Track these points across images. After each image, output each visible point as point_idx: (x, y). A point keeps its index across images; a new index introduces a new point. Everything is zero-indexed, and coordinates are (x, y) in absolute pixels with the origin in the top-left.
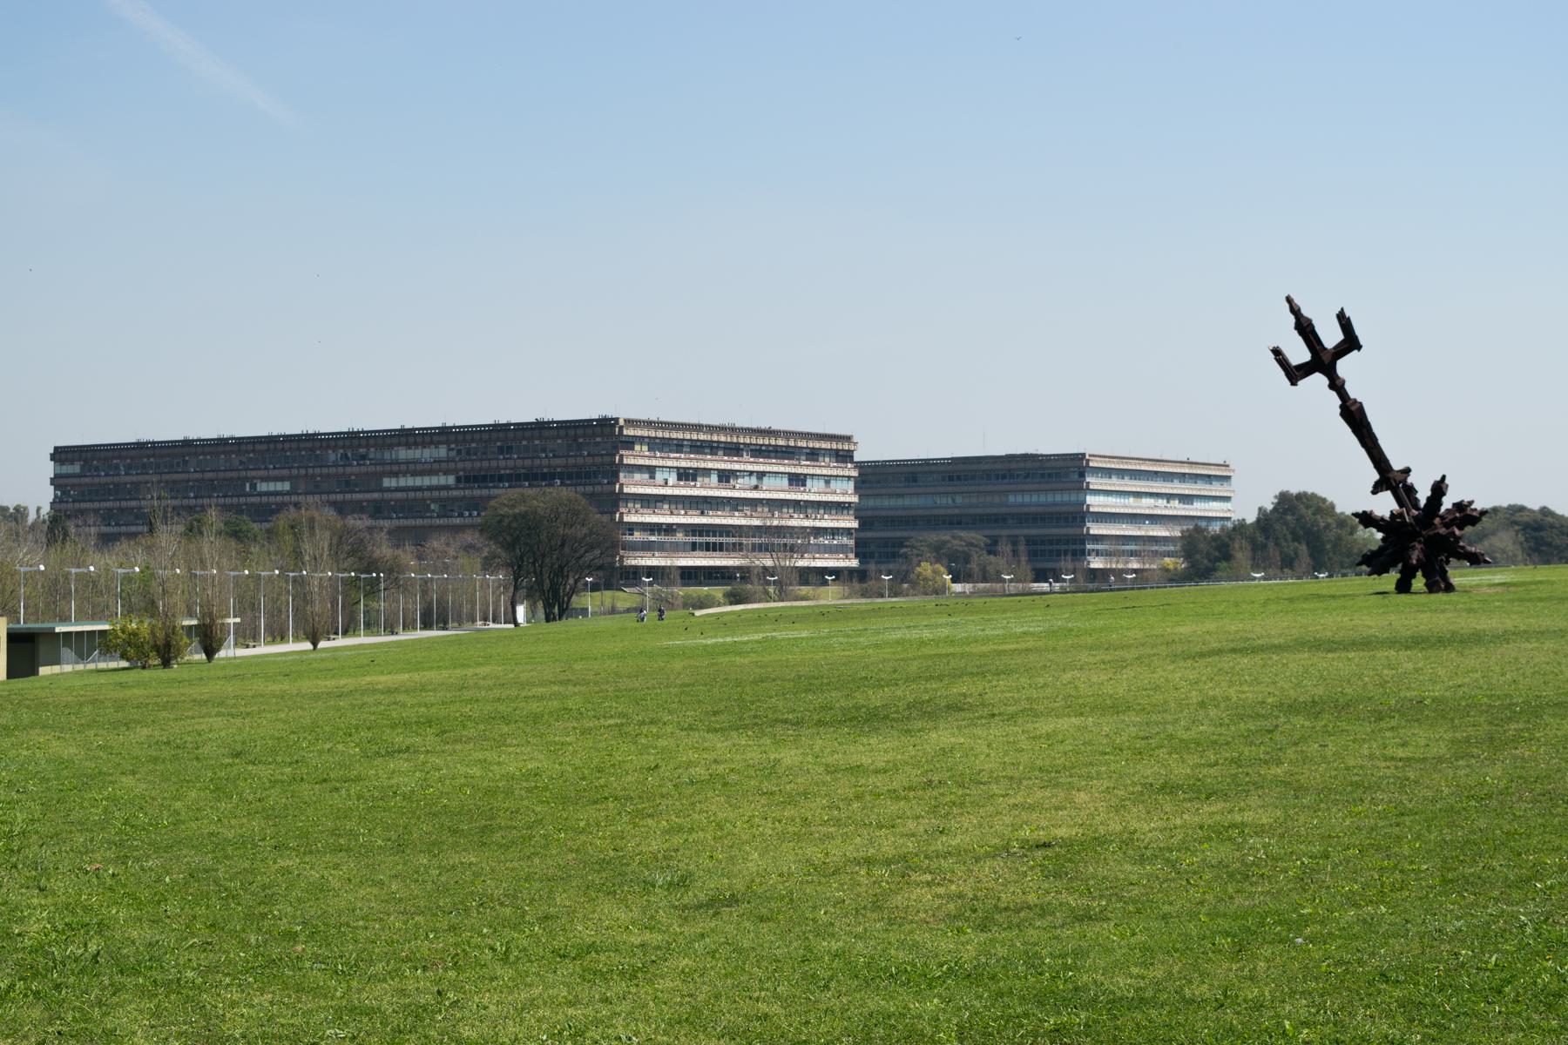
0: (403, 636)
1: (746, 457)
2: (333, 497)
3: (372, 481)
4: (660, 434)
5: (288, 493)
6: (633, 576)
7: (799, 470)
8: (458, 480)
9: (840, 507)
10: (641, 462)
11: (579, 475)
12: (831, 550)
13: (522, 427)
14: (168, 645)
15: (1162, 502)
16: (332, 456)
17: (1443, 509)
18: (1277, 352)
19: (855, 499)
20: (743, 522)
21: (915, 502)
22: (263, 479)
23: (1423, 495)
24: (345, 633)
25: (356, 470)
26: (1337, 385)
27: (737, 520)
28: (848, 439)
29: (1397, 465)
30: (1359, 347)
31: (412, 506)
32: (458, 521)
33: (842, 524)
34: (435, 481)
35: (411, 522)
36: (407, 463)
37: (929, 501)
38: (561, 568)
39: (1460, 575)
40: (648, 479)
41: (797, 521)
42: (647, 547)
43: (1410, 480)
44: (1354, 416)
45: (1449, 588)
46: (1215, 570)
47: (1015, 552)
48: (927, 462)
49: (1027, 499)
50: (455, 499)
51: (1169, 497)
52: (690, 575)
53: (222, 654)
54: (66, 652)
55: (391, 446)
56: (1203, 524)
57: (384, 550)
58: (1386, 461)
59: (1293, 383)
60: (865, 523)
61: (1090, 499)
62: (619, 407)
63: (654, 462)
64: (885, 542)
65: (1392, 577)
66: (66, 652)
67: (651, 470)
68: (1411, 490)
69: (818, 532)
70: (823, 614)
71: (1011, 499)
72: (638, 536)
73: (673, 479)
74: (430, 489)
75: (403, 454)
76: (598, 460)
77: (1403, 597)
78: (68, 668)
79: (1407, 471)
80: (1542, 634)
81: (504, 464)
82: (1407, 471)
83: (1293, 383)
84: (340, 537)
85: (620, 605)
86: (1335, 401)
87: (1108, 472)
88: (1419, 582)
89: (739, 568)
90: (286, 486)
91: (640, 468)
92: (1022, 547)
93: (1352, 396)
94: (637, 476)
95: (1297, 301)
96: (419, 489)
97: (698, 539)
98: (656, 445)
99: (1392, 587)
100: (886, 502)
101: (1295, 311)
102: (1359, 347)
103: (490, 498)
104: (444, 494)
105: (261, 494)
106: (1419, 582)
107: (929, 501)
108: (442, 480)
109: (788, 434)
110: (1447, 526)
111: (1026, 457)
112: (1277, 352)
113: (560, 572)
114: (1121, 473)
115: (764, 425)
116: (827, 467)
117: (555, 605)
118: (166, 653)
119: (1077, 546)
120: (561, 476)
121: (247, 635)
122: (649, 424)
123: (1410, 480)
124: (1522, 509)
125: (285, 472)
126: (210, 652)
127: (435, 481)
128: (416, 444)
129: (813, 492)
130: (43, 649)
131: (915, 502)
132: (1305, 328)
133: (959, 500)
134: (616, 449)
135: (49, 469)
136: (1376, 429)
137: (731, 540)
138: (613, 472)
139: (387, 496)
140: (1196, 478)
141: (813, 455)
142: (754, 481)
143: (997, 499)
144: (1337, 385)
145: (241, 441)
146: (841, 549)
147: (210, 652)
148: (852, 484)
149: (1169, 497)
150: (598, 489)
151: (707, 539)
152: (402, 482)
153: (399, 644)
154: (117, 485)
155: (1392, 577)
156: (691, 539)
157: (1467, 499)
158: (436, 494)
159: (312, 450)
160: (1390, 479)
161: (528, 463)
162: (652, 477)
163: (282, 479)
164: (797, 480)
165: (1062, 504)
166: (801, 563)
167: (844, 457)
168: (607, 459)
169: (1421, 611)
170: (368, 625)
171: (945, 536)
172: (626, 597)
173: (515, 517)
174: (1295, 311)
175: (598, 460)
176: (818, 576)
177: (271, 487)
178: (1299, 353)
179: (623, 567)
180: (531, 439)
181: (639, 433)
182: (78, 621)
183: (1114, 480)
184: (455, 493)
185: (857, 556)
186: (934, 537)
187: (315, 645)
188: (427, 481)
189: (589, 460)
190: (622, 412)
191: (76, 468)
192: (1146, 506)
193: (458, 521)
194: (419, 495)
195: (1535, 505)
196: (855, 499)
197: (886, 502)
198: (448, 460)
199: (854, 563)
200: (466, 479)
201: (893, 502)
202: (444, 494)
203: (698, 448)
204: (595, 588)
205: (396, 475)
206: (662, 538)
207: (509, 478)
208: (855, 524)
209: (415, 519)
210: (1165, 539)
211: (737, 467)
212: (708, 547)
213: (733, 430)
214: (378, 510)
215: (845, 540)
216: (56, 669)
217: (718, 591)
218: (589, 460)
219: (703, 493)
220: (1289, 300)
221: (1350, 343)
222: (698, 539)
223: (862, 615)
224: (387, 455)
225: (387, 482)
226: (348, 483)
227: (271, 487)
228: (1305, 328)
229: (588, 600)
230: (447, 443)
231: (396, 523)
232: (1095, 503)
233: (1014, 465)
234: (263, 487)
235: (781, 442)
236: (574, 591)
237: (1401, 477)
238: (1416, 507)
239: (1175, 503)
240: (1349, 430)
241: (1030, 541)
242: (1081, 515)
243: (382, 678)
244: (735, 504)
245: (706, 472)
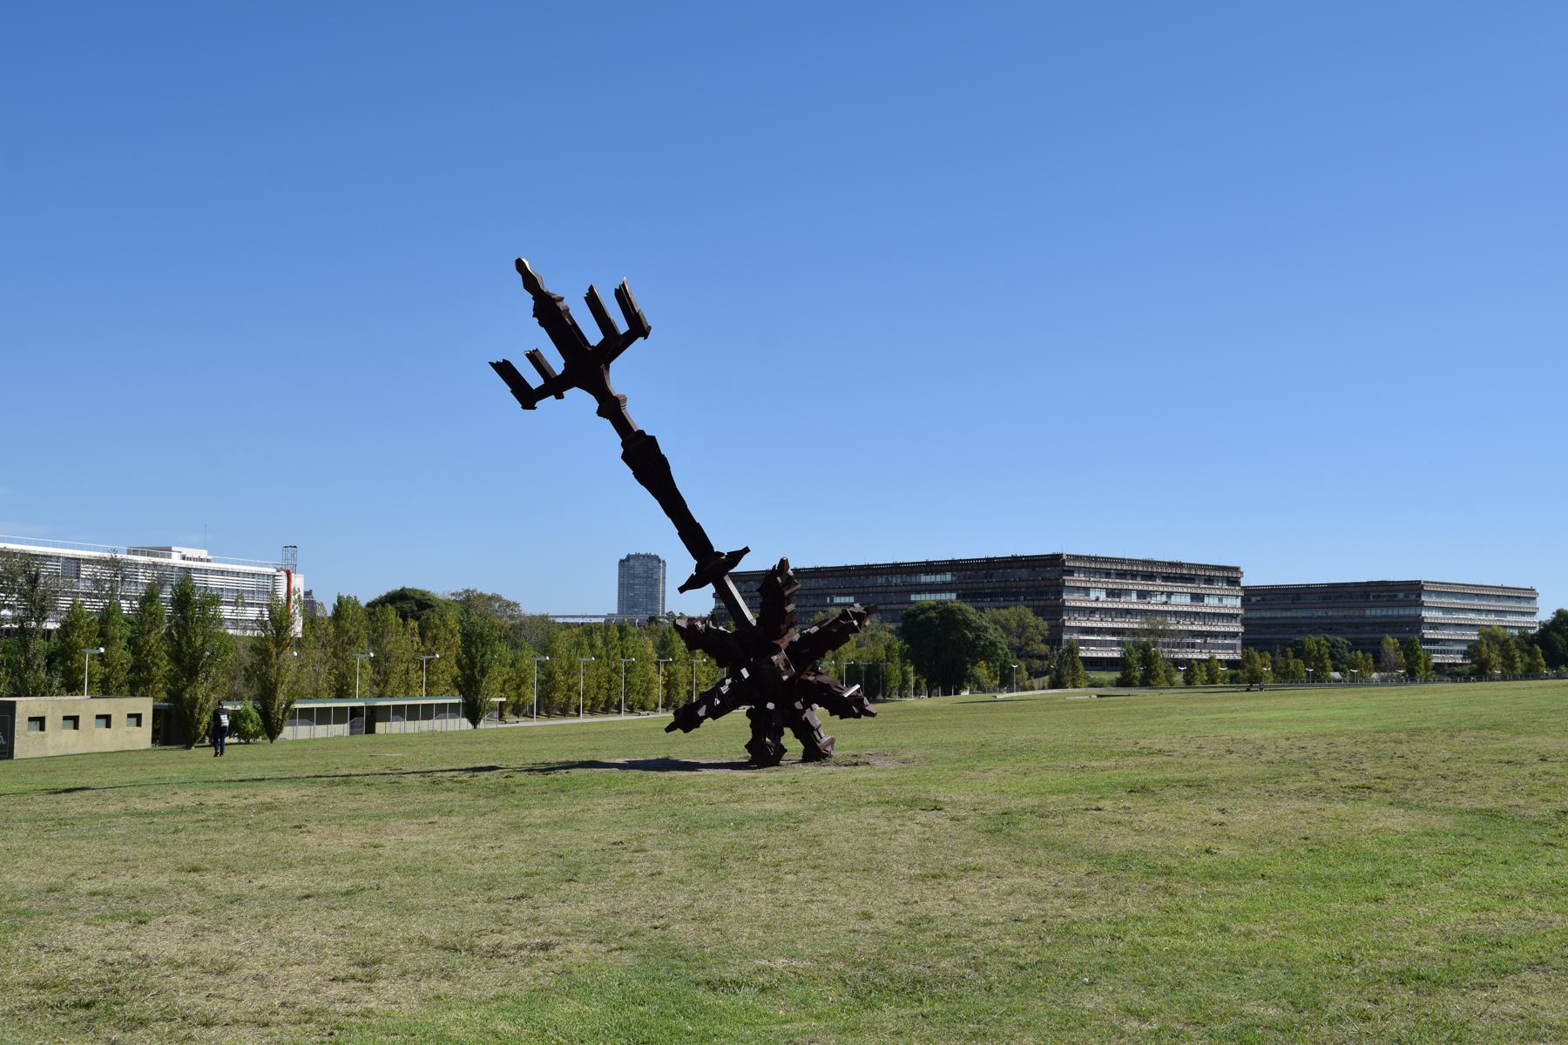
1: (1159, 582)
9: (1232, 617)
26: (611, 408)
28: (1236, 569)
40: (1087, 596)
44: (646, 461)
55: (867, 576)
71: (1368, 612)
73: (1103, 596)
75: (924, 579)
91: (1078, 588)
94: (1076, 596)
101: (530, 282)
109: (1191, 566)
132: (549, 311)
138: (1059, 589)
142: (1164, 598)
144: (611, 408)
146: (1233, 647)
160: (712, 566)
164: (1142, 595)
167: (1234, 582)
174: (530, 282)
182: (330, 699)
201: (1285, 614)
203: (1122, 575)
205: (918, 592)
220: (520, 265)
224: (866, 583)
225: (913, 597)
228: (549, 311)
242: (1419, 623)
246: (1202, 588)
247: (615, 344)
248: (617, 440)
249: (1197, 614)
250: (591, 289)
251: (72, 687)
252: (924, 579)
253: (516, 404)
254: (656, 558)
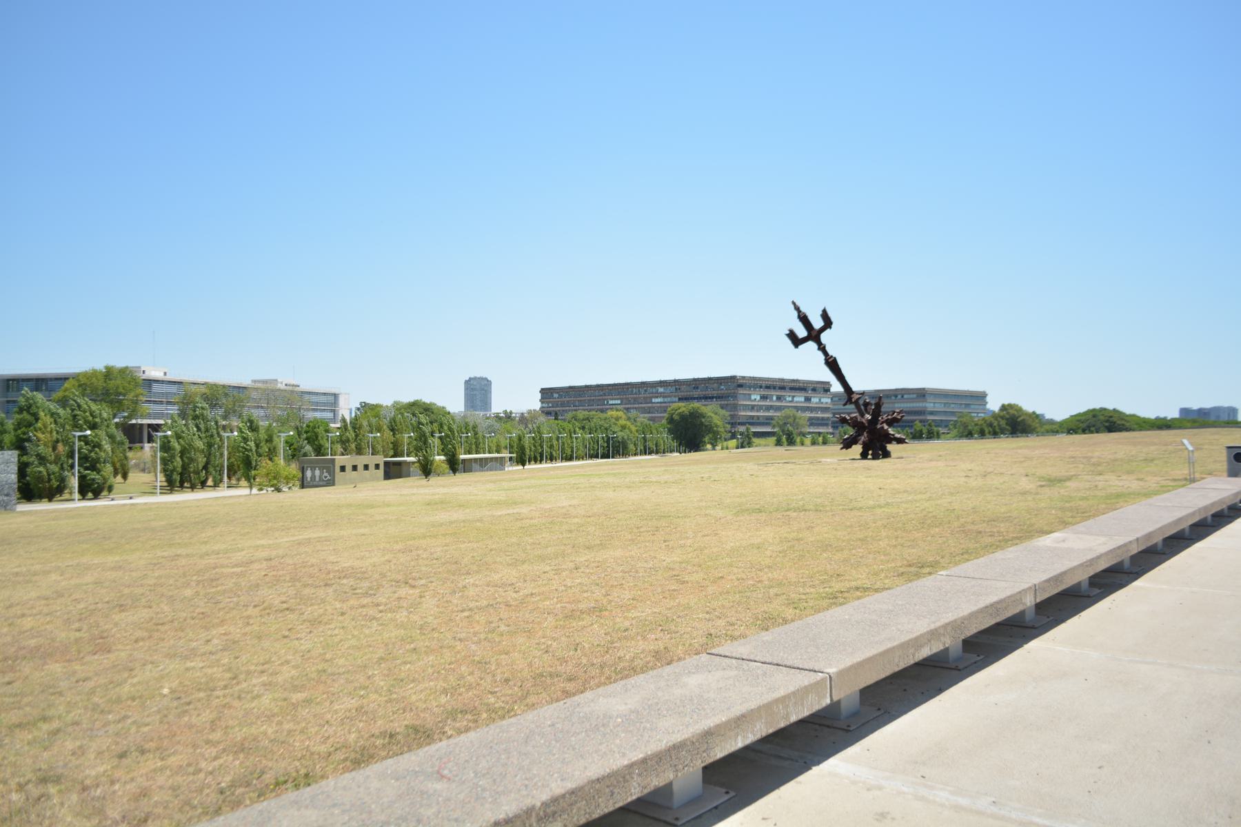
3: (648, 400)
9: (825, 410)
26: (822, 348)
81: (696, 393)
101: (797, 309)
132: (804, 319)
135: (539, 396)
144: (822, 348)
153: (117, 506)
174: (797, 309)
178: (802, 332)
195: (1111, 408)
203: (768, 387)
220: (794, 303)
221: (828, 323)
228: (804, 319)
246: (810, 394)
247: (823, 330)
250: (824, 312)
251: (359, 451)
253: (792, 346)
254: (466, 382)
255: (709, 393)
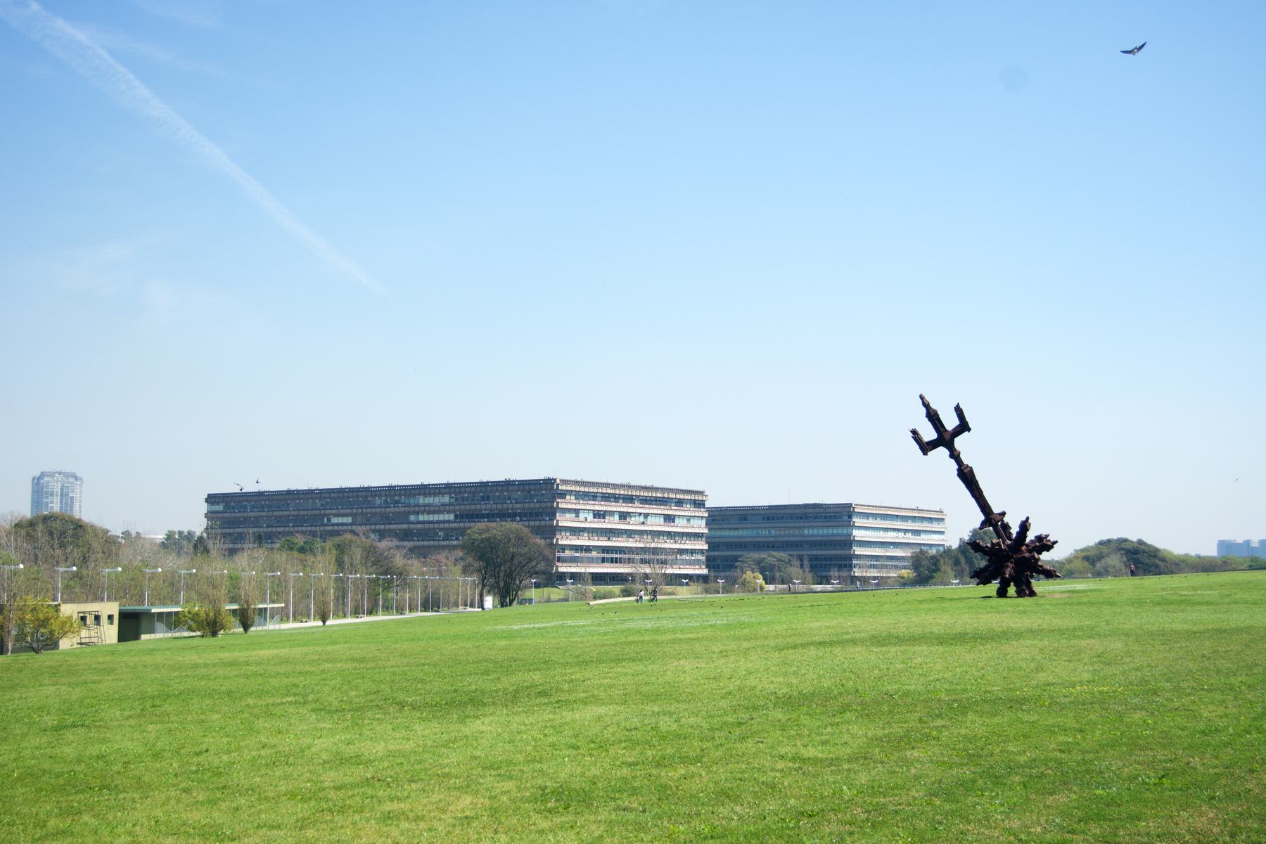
0: (408, 615)
1: (637, 504)
2: (378, 527)
3: (403, 517)
4: (582, 489)
5: (351, 524)
6: (562, 578)
7: (671, 513)
8: (456, 517)
9: (697, 536)
10: (570, 506)
11: (531, 515)
12: (690, 563)
13: (497, 484)
14: (215, 622)
15: (901, 534)
16: (378, 501)
17: (1028, 540)
18: (914, 432)
19: (706, 531)
20: (634, 545)
21: (745, 533)
22: (335, 515)
23: (1015, 530)
24: (370, 613)
25: (392, 510)
26: (955, 455)
27: (630, 543)
28: (702, 493)
29: (996, 509)
30: (969, 430)
31: (427, 533)
32: (455, 543)
33: (698, 547)
34: (441, 517)
35: (426, 543)
36: (425, 506)
37: (754, 533)
38: (511, 572)
39: (1039, 585)
40: (574, 517)
41: (670, 545)
42: (573, 560)
43: (1006, 519)
44: (967, 477)
45: (1032, 594)
46: (932, 577)
47: (802, 566)
48: (753, 508)
49: (816, 532)
50: (454, 529)
51: (906, 531)
52: (598, 578)
53: (253, 629)
54: (158, 625)
55: (414, 496)
56: (924, 548)
57: (399, 561)
58: (989, 507)
59: (925, 454)
60: (713, 546)
61: (855, 532)
62: (557, 472)
63: (578, 507)
64: (726, 558)
65: (995, 585)
66: (158, 625)
67: (577, 512)
68: (1006, 527)
69: (681, 551)
70: (683, 603)
71: (806, 532)
72: (568, 553)
73: (590, 517)
74: (438, 522)
76: (543, 505)
77: (1003, 600)
78: (159, 636)
79: (1003, 514)
80: (1033, 633)
81: (485, 507)
82: (1003, 514)
83: (925, 454)
84: (370, 551)
85: (553, 597)
86: (954, 466)
87: (867, 515)
88: (1012, 590)
89: (631, 574)
90: (349, 520)
91: (569, 510)
92: (806, 562)
93: (965, 462)
94: (568, 516)
95: (927, 398)
96: (432, 522)
97: (605, 555)
98: (580, 496)
99: (994, 593)
100: (727, 533)
102: (969, 430)
103: (465, 529)
104: (447, 525)
105: (334, 525)
106: (1012, 590)
107: (754, 533)
108: (447, 517)
109: (664, 490)
110: (1030, 551)
111: (815, 506)
112: (914, 432)
113: (510, 576)
114: (875, 516)
115: (649, 484)
116: (688, 510)
117: (507, 596)
118: (212, 627)
119: (846, 562)
120: (520, 515)
121: (336, 615)
122: (577, 483)
123: (1006, 519)
124: (1126, 540)
125: (349, 511)
126: (246, 627)
127: (441, 517)
128: (430, 494)
129: (680, 526)
130: (144, 623)
131: (745, 533)
132: (933, 417)
133: (773, 532)
134: (554, 498)
135: (204, 508)
136: (982, 485)
137: (627, 556)
139: (412, 526)
140: (922, 519)
141: (680, 503)
142: (642, 519)
143: (797, 532)
144: (955, 455)
145: (322, 491)
146: (697, 562)
147: (246, 627)
148: (704, 522)
149: (906, 531)
150: (543, 523)
151: (612, 555)
152: (421, 518)
154: (245, 518)
155: (995, 585)
156: (602, 555)
157: (1044, 534)
158: (442, 526)
159: (366, 497)
161: (500, 506)
162: (577, 516)
163: (346, 515)
164: (669, 519)
165: (838, 535)
166: (669, 571)
167: (699, 504)
168: (549, 505)
169: (1011, 612)
170: (294, 617)
171: (763, 555)
172: (556, 592)
173: (482, 541)
175: (543, 505)
176: (676, 580)
177: (340, 520)
178: (929, 434)
179: (557, 572)
180: (502, 491)
181: (569, 488)
183: (871, 520)
184: (454, 525)
185: (707, 567)
186: (756, 555)
187: (324, 622)
188: (436, 517)
189: (538, 505)
190: (558, 476)
191: (220, 508)
192: (891, 537)
193: (455, 543)
194: (431, 526)
195: (1134, 538)
196: (706, 531)
197: (727, 533)
198: (450, 504)
199: (705, 571)
200: (460, 517)
201: (731, 533)
202: (447, 525)
203: (606, 498)
204: (537, 586)
206: (584, 555)
207: (488, 516)
208: (706, 547)
209: (423, 541)
210: (902, 557)
211: (631, 510)
212: (613, 561)
213: (629, 487)
214: (405, 535)
215: (699, 557)
216: (152, 636)
217: (616, 589)
218: (538, 505)
219: (609, 526)
220: (922, 397)
221: (963, 427)
222: (605, 555)
223: (702, 604)
224: (412, 501)
226: (388, 518)
227: (340, 520)
228: (933, 417)
229: (533, 593)
230: (449, 493)
231: (412, 544)
232: (858, 535)
233: (808, 511)
234: (335, 520)
235: (659, 495)
236: (519, 588)
237: (999, 518)
238: (1010, 539)
239: (909, 535)
240: (963, 486)
241: (813, 559)
242: (849, 543)
243: (263, 652)
244: (630, 534)
245: (612, 513)
248: (956, 467)
249: (669, 533)
252: (421, 500)
255: (508, 506)
